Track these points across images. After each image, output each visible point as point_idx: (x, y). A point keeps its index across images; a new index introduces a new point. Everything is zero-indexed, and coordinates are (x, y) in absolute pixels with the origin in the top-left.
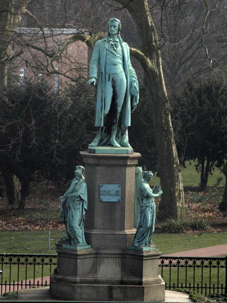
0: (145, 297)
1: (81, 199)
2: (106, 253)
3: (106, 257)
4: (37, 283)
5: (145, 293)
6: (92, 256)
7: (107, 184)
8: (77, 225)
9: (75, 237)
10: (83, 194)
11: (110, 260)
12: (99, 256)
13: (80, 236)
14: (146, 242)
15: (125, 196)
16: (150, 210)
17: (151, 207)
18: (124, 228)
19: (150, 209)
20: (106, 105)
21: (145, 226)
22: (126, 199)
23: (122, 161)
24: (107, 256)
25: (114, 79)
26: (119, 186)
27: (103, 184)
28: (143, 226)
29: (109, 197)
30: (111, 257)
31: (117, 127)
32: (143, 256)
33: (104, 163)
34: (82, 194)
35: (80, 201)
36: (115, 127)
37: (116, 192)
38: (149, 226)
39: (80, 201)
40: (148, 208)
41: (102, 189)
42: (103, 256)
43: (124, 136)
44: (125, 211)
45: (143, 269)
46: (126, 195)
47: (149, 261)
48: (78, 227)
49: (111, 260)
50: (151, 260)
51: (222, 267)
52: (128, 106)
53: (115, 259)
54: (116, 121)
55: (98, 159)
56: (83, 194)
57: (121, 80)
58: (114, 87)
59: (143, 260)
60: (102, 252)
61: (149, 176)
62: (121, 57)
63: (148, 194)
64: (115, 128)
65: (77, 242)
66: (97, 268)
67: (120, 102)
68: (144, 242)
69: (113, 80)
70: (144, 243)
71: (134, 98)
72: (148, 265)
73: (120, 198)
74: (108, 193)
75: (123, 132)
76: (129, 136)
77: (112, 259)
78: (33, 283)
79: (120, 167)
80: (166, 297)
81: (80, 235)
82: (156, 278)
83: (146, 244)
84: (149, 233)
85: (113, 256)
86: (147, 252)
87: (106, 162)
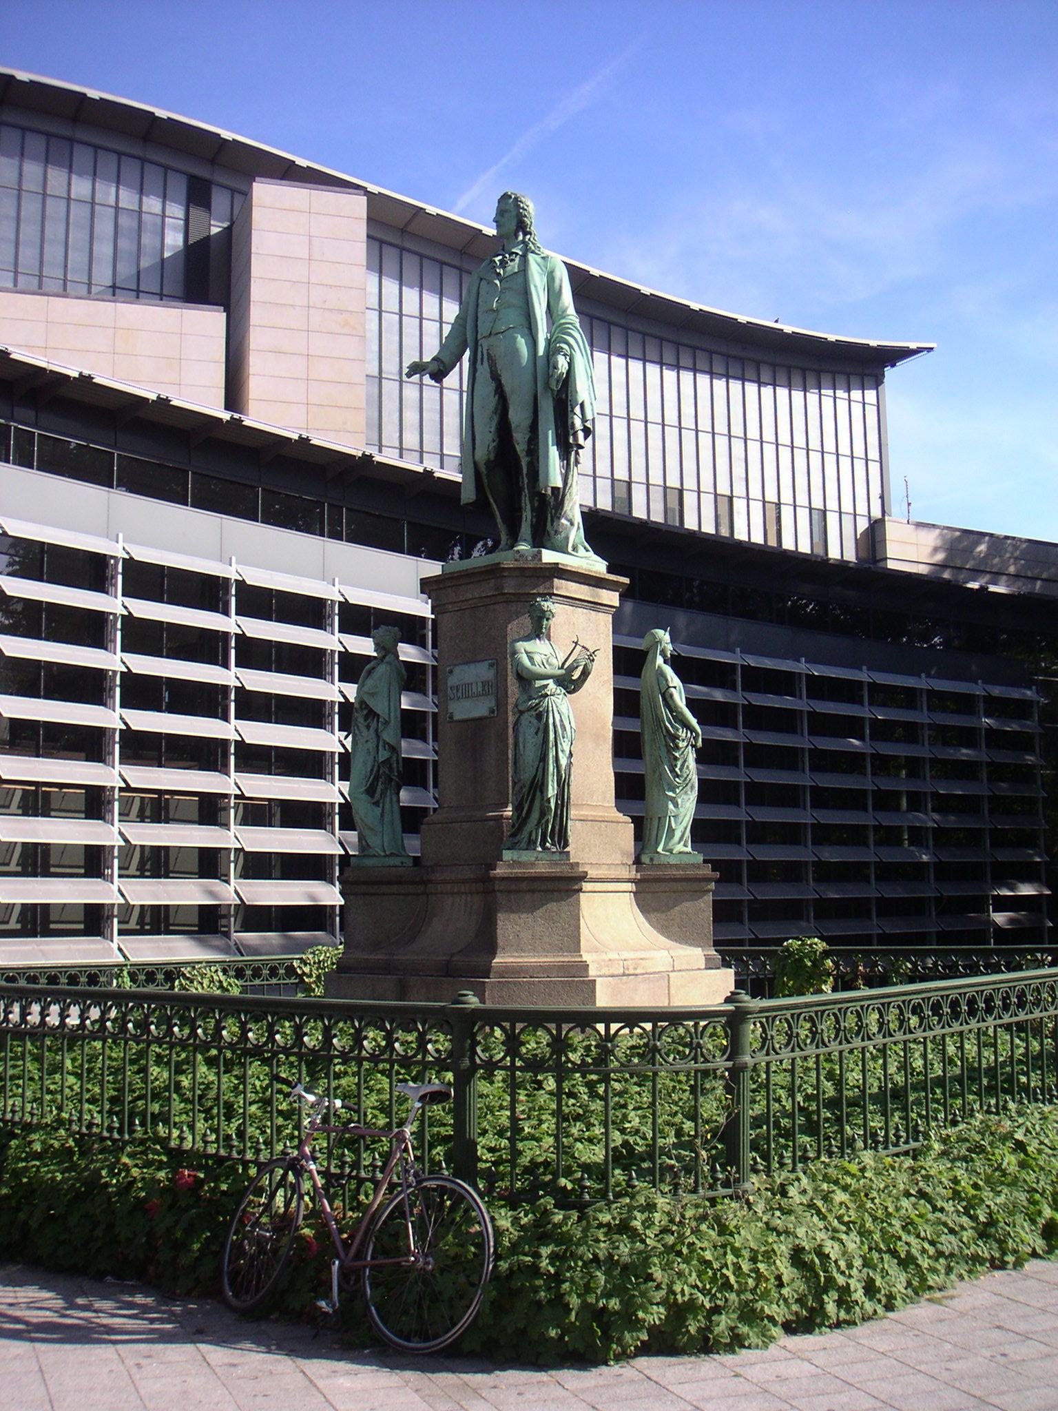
7: (467, 663)
46: (509, 692)
58: (496, 377)
67: (518, 416)
69: (488, 354)
73: (493, 704)
76: (328, 908)
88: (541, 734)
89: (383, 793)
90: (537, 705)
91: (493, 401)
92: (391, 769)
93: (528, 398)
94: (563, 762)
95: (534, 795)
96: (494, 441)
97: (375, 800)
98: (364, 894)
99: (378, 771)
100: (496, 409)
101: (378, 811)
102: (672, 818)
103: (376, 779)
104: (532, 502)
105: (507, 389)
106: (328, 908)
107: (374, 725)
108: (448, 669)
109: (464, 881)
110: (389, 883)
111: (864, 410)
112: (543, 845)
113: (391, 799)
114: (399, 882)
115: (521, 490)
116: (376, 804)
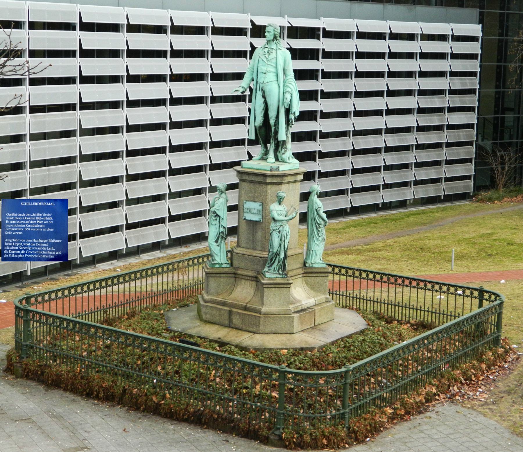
6: (301, 276)
11: (247, 281)
12: (237, 276)
23: (262, 177)
24: (244, 277)
29: (252, 215)
37: (258, 210)
41: (245, 206)
49: (248, 283)
51: (476, 298)
58: (264, 97)
62: (274, 65)
67: (272, 114)
69: (262, 89)
73: (261, 217)
74: (251, 212)
76: (108, 132)
80: (225, 336)
88: (280, 237)
89: (221, 242)
91: (263, 105)
92: (223, 234)
93: (276, 108)
94: (286, 246)
101: (219, 248)
103: (219, 237)
104: (274, 142)
105: (269, 103)
106: (108, 132)
107: (218, 219)
110: (224, 273)
114: (227, 273)
115: (271, 137)
116: (218, 246)
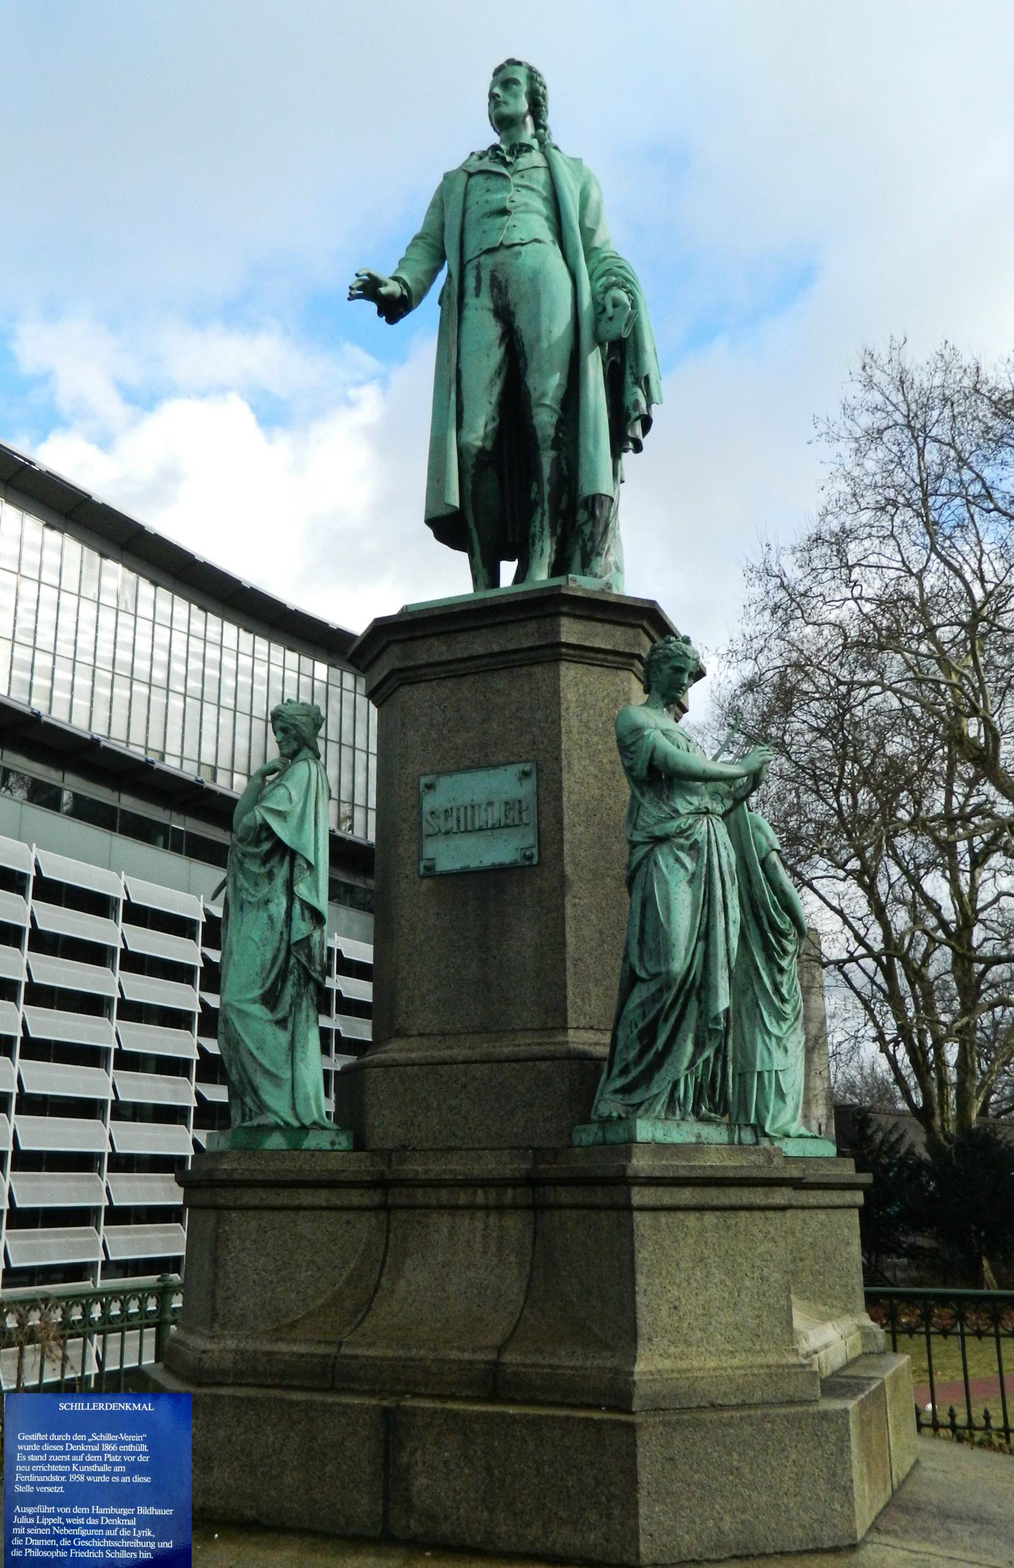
0: (642, 1511)
1: (282, 851)
2: (432, 1176)
3: (440, 1207)
4: (949, 1420)
5: (644, 1476)
7: (468, 769)
8: (253, 1002)
9: (245, 1080)
10: (293, 821)
11: (464, 1222)
12: (398, 1196)
13: (273, 1070)
14: (676, 1085)
15: (561, 829)
16: (683, 866)
17: (688, 843)
18: (565, 1020)
19: (678, 859)
20: (465, 403)
21: (653, 970)
22: (566, 847)
25: (500, 276)
26: (526, 774)
27: (439, 774)
28: (643, 974)
30: (471, 1207)
31: (546, 518)
32: (625, 1181)
33: (436, 658)
34: (281, 815)
35: (274, 861)
36: (538, 524)
38: (679, 965)
39: (277, 858)
40: (665, 848)
42: (420, 1196)
43: (593, 563)
44: (563, 918)
45: (641, 1280)
46: (566, 821)
47: (692, 1219)
48: (258, 1010)
50: (710, 1219)
52: (587, 397)
53: (493, 1219)
54: (540, 491)
55: (405, 641)
56: (293, 821)
57: (536, 279)
58: (504, 314)
59: (630, 1208)
60: (414, 1168)
61: (667, 658)
63: (653, 753)
64: (538, 529)
65: (255, 1109)
66: (384, 1280)
68: (660, 1085)
69: (494, 278)
70: (664, 1098)
71: (628, 371)
72: (687, 1251)
73: (531, 839)
75: (589, 545)
77: (480, 1214)
78: (965, 1417)
79: (524, 670)
81: (274, 1063)
82: (772, 1359)
83: (672, 1102)
84: (691, 1021)
85: (480, 1197)
86: (661, 1148)
87: (444, 648)
89: (295, 1005)
90: (690, 827)
95: (685, 1006)
96: (494, 419)
97: (280, 1015)
98: (257, 1208)
99: (287, 960)
100: (500, 367)
102: (780, 1075)
103: (283, 976)
108: (424, 780)
109: (485, 1183)
110: (317, 1184)
111: (219, 714)
112: (696, 1111)
113: (308, 1016)
114: (333, 1184)
116: (282, 1023)
